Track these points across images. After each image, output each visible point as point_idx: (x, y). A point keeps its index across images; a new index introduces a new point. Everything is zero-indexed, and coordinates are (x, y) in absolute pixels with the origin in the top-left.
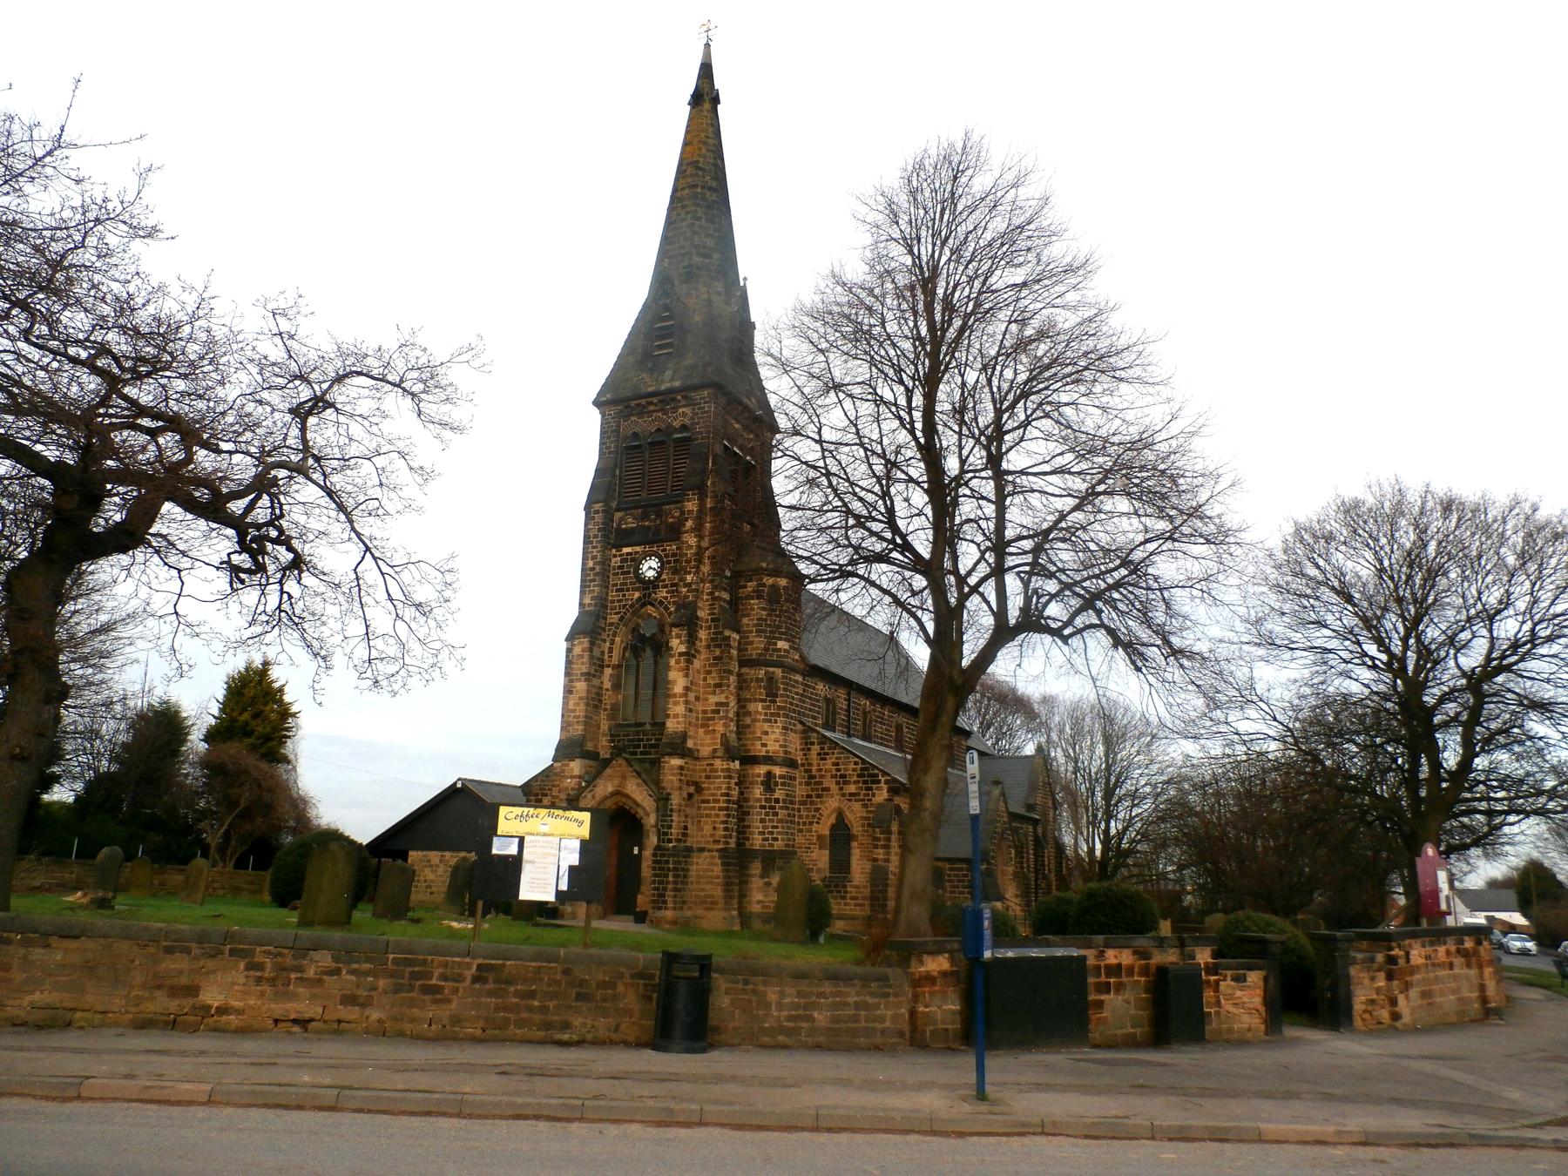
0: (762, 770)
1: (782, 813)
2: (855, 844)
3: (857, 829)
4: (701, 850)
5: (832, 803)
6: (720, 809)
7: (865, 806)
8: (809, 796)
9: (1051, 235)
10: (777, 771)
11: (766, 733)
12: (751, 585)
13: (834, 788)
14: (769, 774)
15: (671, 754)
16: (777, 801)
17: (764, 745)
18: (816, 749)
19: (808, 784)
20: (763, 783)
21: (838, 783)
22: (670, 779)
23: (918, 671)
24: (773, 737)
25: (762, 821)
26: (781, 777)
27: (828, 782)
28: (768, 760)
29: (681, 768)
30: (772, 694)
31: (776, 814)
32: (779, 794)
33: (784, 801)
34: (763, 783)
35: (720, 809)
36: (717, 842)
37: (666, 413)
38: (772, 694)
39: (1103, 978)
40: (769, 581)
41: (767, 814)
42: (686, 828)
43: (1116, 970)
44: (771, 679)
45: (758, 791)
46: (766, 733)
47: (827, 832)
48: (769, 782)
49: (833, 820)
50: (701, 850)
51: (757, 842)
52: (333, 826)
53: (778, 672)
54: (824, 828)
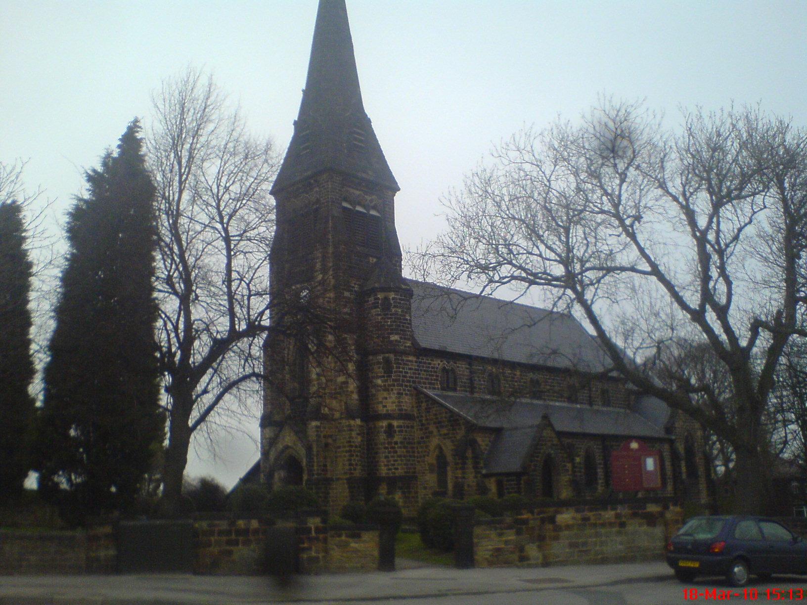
0: (384, 424)
1: (400, 451)
2: (449, 468)
3: (449, 458)
4: (338, 479)
5: (435, 441)
6: (346, 452)
7: (453, 441)
8: (422, 438)
9: (94, 171)
10: (395, 423)
11: (386, 398)
12: (371, 300)
13: (435, 431)
14: (390, 426)
15: (312, 419)
16: (396, 443)
17: (385, 406)
18: (424, 405)
19: (421, 430)
20: (385, 432)
21: (437, 427)
22: (312, 434)
23: (596, 337)
24: (391, 400)
25: (386, 457)
26: (398, 427)
27: (432, 428)
28: (388, 416)
29: (317, 427)
30: (388, 371)
31: (396, 452)
32: (397, 438)
33: (401, 443)
34: (385, 432)
35: (346, 452)
36: (345, 473)
37: (307, 193)
38: (388, 371)
39: (233, 537)
40: (380, 296)
41: (389, 452)
42: (325, 466)
43: (246, 532)
44: (387, 361)
45: (383, 437)
46: (386, 398)
47: (434, 462)
48: (390, 431)
49: (437, 452)
50: (338, 479)
51: (383, 471)
52: (213, 480)
53: (392, 356)
54: (431, 459)
